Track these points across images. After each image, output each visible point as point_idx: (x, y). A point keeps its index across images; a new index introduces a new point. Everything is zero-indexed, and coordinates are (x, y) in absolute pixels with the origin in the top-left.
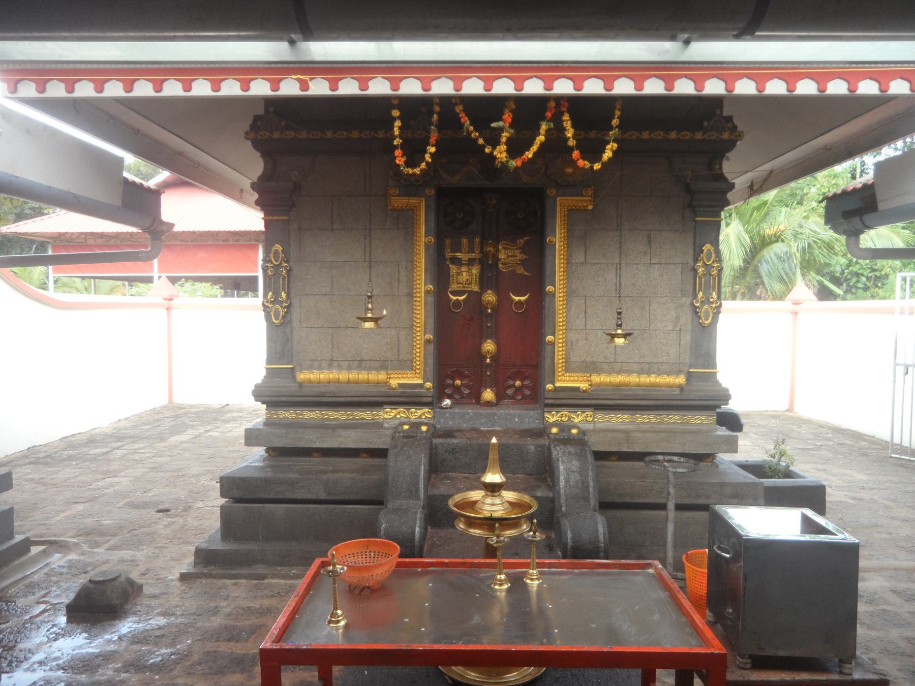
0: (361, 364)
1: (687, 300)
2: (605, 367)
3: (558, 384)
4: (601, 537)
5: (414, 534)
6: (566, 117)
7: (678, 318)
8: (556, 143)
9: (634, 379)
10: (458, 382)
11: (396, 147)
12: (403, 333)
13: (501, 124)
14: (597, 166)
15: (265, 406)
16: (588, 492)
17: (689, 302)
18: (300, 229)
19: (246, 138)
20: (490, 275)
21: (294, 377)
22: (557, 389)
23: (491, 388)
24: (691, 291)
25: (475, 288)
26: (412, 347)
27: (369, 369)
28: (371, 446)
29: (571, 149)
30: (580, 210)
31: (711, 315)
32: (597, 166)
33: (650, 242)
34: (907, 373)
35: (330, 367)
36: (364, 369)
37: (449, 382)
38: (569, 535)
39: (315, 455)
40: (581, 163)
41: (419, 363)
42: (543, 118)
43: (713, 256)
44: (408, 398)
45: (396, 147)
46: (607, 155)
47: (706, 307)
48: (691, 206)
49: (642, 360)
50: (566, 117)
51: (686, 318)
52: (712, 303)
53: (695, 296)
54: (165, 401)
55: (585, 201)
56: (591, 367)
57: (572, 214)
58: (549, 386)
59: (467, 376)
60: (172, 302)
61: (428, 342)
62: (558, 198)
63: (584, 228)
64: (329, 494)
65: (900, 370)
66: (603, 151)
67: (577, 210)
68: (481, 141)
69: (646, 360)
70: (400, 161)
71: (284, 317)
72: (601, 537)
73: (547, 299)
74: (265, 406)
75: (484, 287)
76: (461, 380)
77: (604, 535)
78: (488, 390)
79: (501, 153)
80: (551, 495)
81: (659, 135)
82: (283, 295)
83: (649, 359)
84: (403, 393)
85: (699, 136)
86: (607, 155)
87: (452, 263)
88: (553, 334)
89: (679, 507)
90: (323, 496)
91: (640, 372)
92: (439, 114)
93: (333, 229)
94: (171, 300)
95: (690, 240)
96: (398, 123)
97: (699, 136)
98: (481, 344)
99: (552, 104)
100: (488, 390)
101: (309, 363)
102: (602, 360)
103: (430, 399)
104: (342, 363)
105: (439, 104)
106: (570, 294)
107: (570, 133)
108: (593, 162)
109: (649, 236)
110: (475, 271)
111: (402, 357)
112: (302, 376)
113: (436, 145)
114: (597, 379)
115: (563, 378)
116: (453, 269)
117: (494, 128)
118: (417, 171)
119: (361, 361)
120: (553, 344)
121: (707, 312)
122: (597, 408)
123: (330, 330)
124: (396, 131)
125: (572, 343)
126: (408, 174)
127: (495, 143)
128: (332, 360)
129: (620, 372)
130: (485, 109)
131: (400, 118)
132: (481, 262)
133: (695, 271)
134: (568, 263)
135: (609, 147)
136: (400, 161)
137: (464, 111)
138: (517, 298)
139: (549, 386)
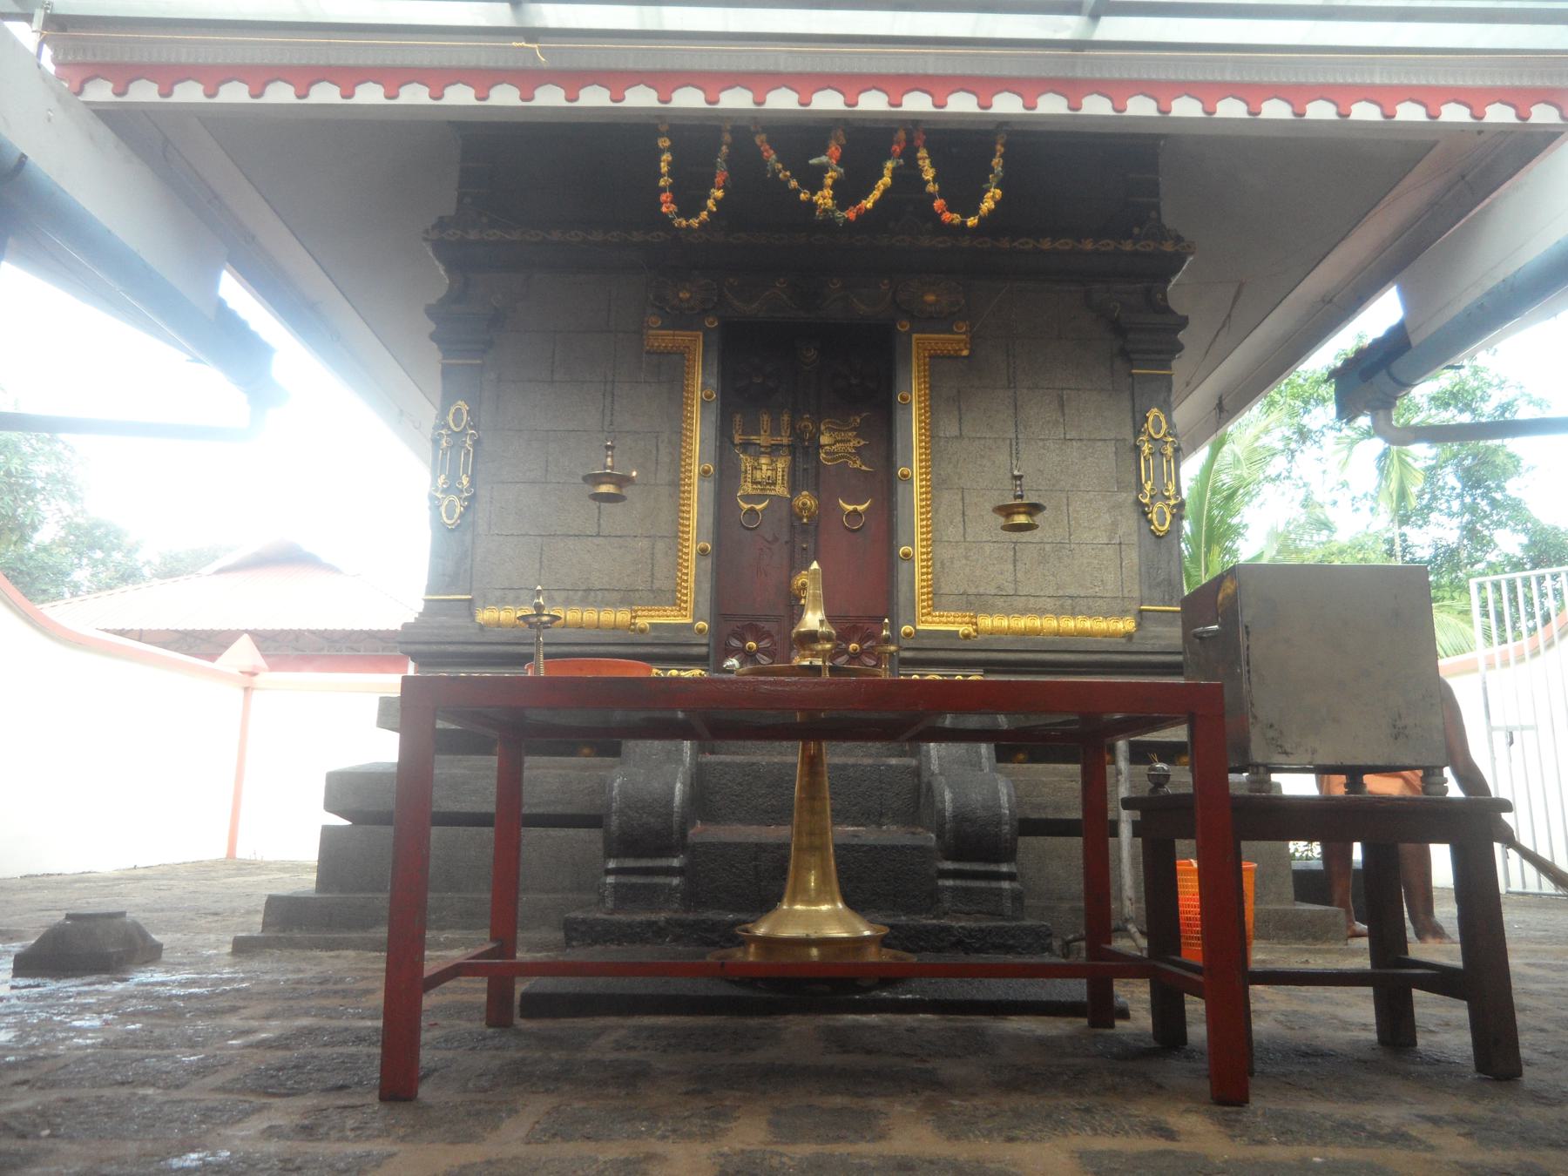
1: (1127, 497)
3: (920, 627)
4: (1004, 799)
5: (672, 799)
6: (923, 153)
7: (1115, 524)
8: (908, 177)
9: (1050, 623)
10: (752, 644)
11: (663, 190)
12: (661, 545)
13: (824, 159)
14: (972, 221)
17: (1131, 498)
19: (426, 240)
20: (805, 465)
21: (472, 615)
24: (1134, 480)
25: (781, 490)
26: (677, 566)
29: (932, 197)
30: (950, 357)
31: (1169, 517)
32: (972, 221)
33: (1062, 406)
34: (1511, 743)
36: (591, 605)
38: (948, 796)
40: (947, 217)
41: (689, 594)
42: (889, 157)
43: (1164, 426)
45: (663, 190)
46: (987, 205)
47: (1159, 504)
48: (1126, 355)
49: (1061, 593)
50: (923, 153)
51: (1129, 523)
52: (1168, 498)
53: (1140, 487)
54: (221, 854)
55: (955, 341)
56: (975, 603)
57: (938, 363)
59: (769, 635)
60: (256, 679)
62: (915, 336)
63: (957, 385)
65: (1500, 739)
66: (981, 200)
68: (793, 184)
69: (1069, 592)
70: (668, 208)
71: (462, 515)
72: (1004, 799)
73: (900, 488)
75: (794, 488)
76: (757, 641)
77: (1009, 795)
79: (824, 198)
80: (914, 762)
81: (1064, 244)
82: (465, 481)
83: (1071, 591)
85: (1128, 246)
86: (987, 205)
87: (744, 452)
91: (1058, 613)
92: (729, 146)
93: (553, 382)
94: (253, 674)
95: (1127, 404)
96: (667, 157)
97: (1128, 246)
98: (790, 578)
99: (901, 135)
101: (498, 593)
103: (704, 650)
104: (555, 594)
105: (731, 132)
106: (936, 486)
107: (929, 174)
108: (966, 215)
110: (781, 464)
111: (657, 584)
112: (485, 615)
113: (724, 187)
114: (986, 622)
115: (929, 618)
116: (746, 461)
117: (813, 166)
118: (694, 222)
119: (588, 590)
121: (1162, 513)
124: (664, 168)
125: (942, 563)
126: (680, 229)
127: (816, 186)
129: (1024, 612)
130: (802, 136)
131: (669, 149)
132: (792, 449)
133: (1137, 449)
134: (932, 437)
135: (989, 195)
136: (668, 208)
137: (769, 142)
138: (850, 508)
139: (907, 628)
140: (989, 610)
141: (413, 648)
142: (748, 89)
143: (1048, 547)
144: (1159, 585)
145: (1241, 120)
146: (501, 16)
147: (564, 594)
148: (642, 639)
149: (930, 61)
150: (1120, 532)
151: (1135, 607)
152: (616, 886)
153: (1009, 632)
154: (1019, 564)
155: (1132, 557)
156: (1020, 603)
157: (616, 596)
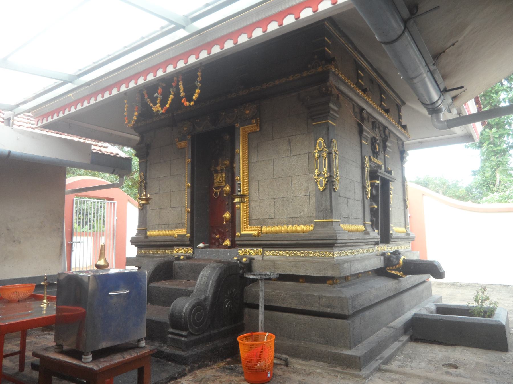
0: (168, 226)
2: (270, 221)
3: (242, 233)
7: (308, 187)
9: (283, 228)
14: (192, 103)
15: (137, 247)
16: (208, 288)
21: (146, 233)
22: (241, 235)
23: (229, 238)
33: (290, 143)
37: (213, 236)
44: (180, 243)
55: (253, 127)
57: (250, 136)
58: (238, 234)
67: (253, 133)
72: (184, 310)
74: (137, 247)
89: (267, 308)
91: (288, 224)
102: (268, 217)
103: (188, 243)
108: (190, 102)
109: (289, 140)
114: (265, 229)
120: (239, 209)
122: (265, 246)
127: (155, 104)
129: (277, 224)
140: (266, 225)
141: (137, 244)
142: (231, 39)
143: (285, 199)
144: (322, 211)
145: (262, 35)
150: (309, 191)
153: (271, 232)
154: (276, 207)
155: (313, 200)
156: (275, 221)
157: (174, 226)
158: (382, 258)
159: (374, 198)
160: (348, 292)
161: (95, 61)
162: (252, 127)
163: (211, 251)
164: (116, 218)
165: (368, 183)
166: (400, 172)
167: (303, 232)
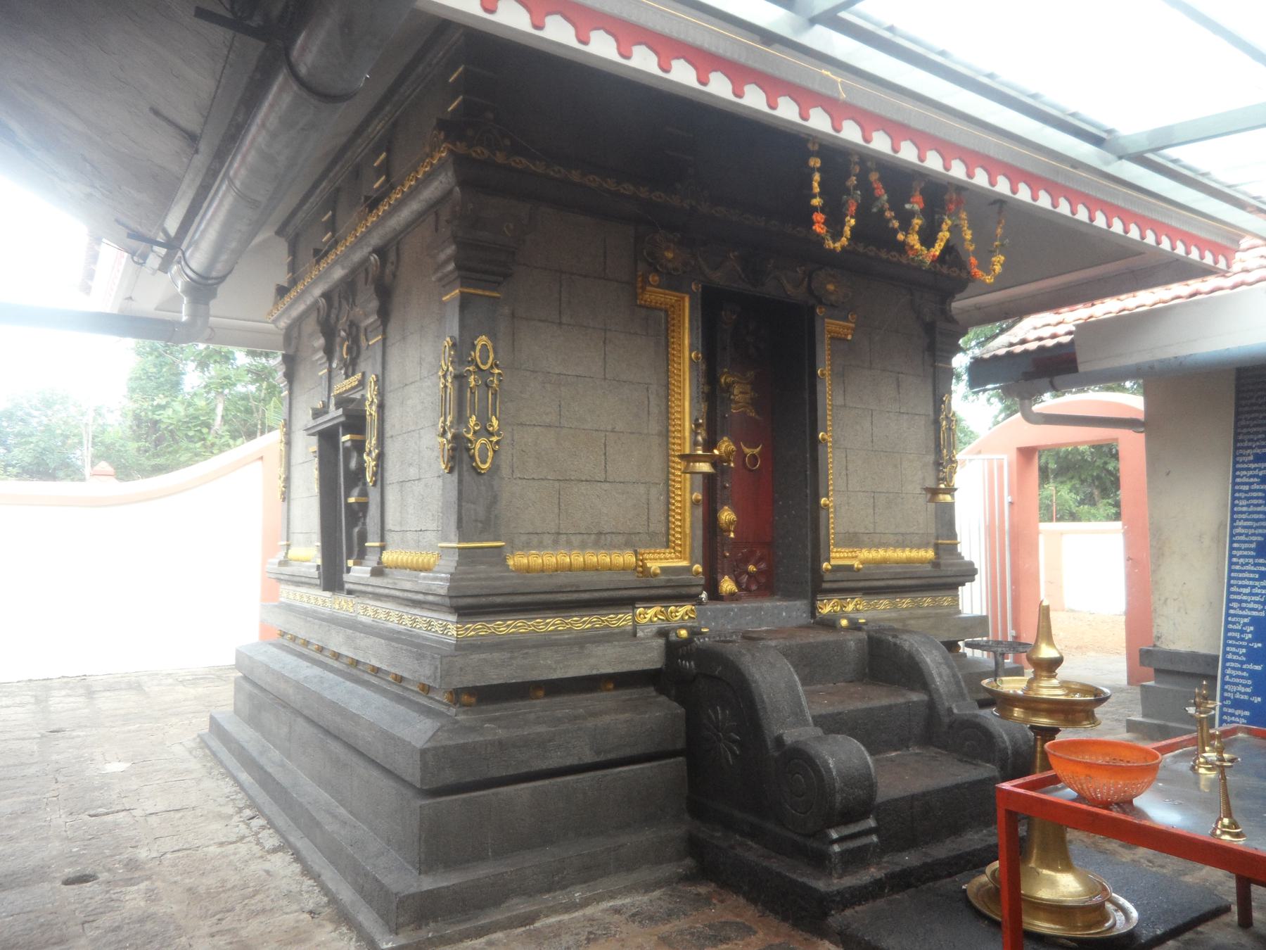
0: (600, 539)
2: (866, 538)
3: (833, 562)
18: (513, 315)
22: (837, 569)
27: (611, 547)
28: (634, 668)
35: (555, 545)
39: (541, 693)
44: (670, 591)
45: (815, 209)
58: (825, 565)
61: (695, 503)
64: (598, 753)
73: (820, 447)
78: (726, 577)
83: (902, 530)
84: (669, 580)
88: (827, 496)
90: (589, 757)
93: (560, 323)
96: (817, 177)
100: (726, 577)
101: (524, 538)
102: (863, 530)
104: (573, 538)
111: (651, 529)
112: (517, 560)
123: (557, 484)
124: (817, 189)
128: (559, 534)
137: (881, 179)
146: (773, 18)
147: (579, 537)
148: (654, 582)
149: (841, 87)
151: (933, 541)
152: (842, 854)
158: (661, 641)
159: (358, 513)
160: (311, 792)
161: (900, 26)
162: (844, 327)
163: (740, 609)
164: (1007, 499)
165: (370, 462)
166: (917, 474)
167: (897, 562)
